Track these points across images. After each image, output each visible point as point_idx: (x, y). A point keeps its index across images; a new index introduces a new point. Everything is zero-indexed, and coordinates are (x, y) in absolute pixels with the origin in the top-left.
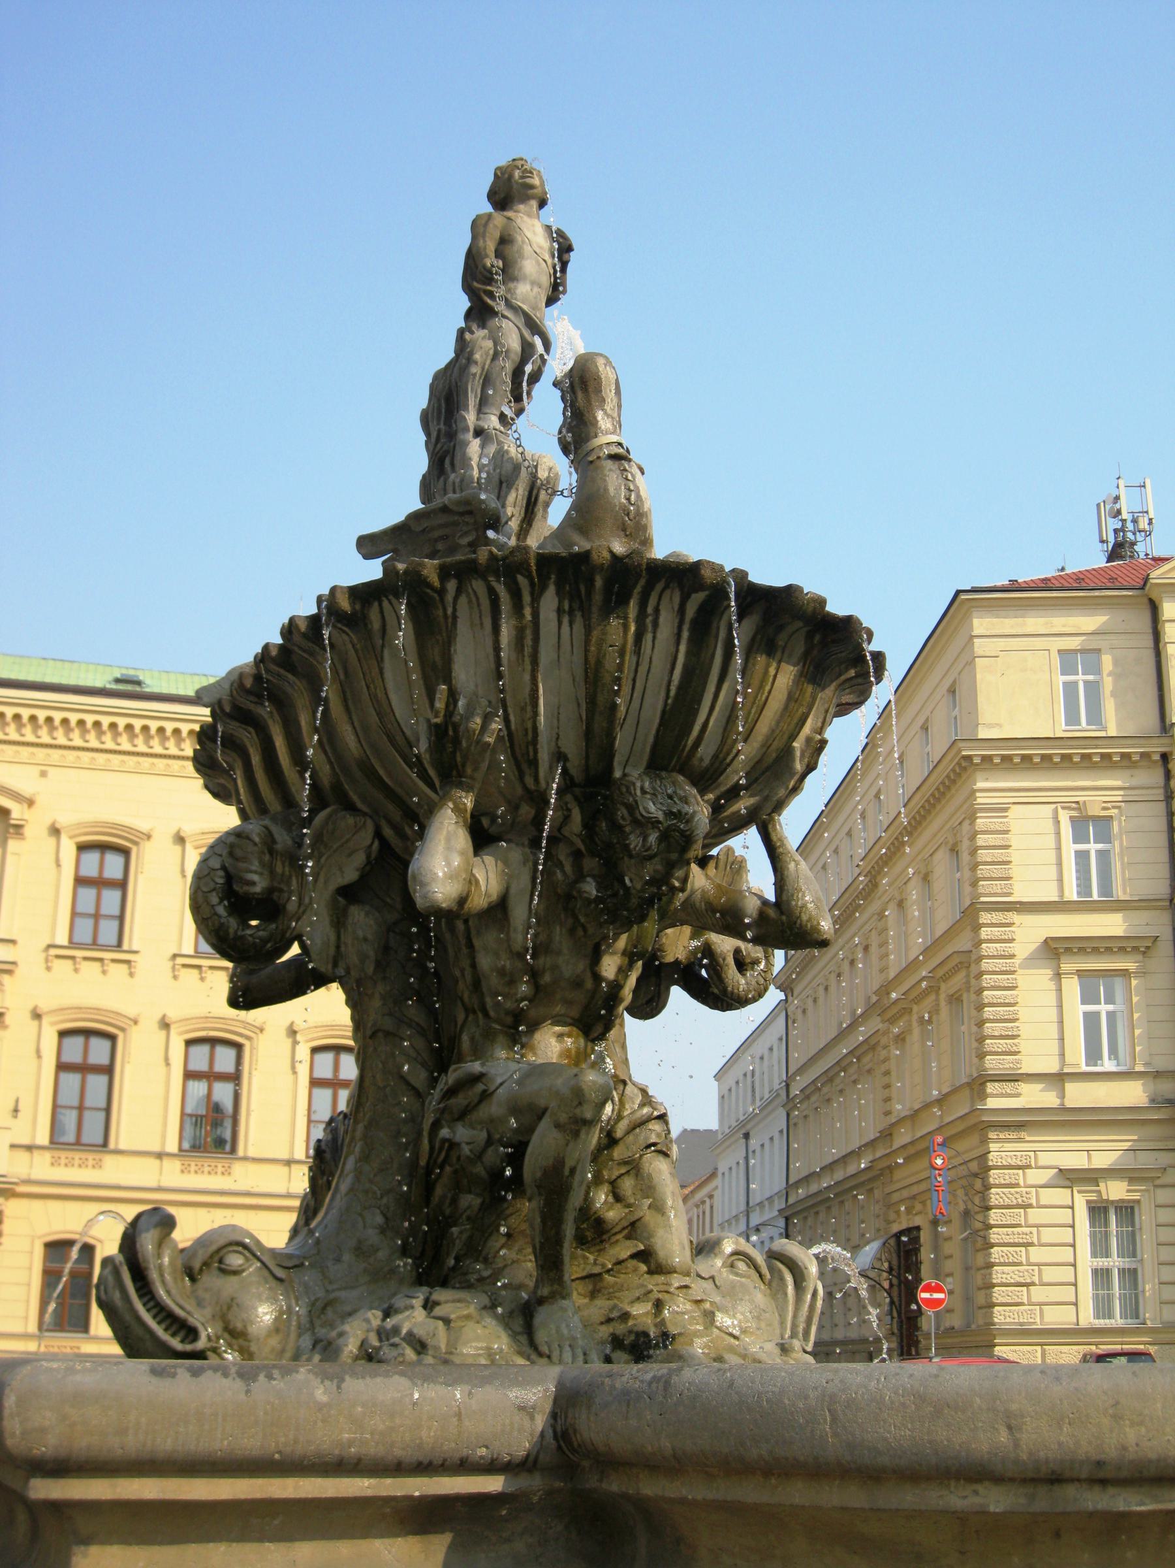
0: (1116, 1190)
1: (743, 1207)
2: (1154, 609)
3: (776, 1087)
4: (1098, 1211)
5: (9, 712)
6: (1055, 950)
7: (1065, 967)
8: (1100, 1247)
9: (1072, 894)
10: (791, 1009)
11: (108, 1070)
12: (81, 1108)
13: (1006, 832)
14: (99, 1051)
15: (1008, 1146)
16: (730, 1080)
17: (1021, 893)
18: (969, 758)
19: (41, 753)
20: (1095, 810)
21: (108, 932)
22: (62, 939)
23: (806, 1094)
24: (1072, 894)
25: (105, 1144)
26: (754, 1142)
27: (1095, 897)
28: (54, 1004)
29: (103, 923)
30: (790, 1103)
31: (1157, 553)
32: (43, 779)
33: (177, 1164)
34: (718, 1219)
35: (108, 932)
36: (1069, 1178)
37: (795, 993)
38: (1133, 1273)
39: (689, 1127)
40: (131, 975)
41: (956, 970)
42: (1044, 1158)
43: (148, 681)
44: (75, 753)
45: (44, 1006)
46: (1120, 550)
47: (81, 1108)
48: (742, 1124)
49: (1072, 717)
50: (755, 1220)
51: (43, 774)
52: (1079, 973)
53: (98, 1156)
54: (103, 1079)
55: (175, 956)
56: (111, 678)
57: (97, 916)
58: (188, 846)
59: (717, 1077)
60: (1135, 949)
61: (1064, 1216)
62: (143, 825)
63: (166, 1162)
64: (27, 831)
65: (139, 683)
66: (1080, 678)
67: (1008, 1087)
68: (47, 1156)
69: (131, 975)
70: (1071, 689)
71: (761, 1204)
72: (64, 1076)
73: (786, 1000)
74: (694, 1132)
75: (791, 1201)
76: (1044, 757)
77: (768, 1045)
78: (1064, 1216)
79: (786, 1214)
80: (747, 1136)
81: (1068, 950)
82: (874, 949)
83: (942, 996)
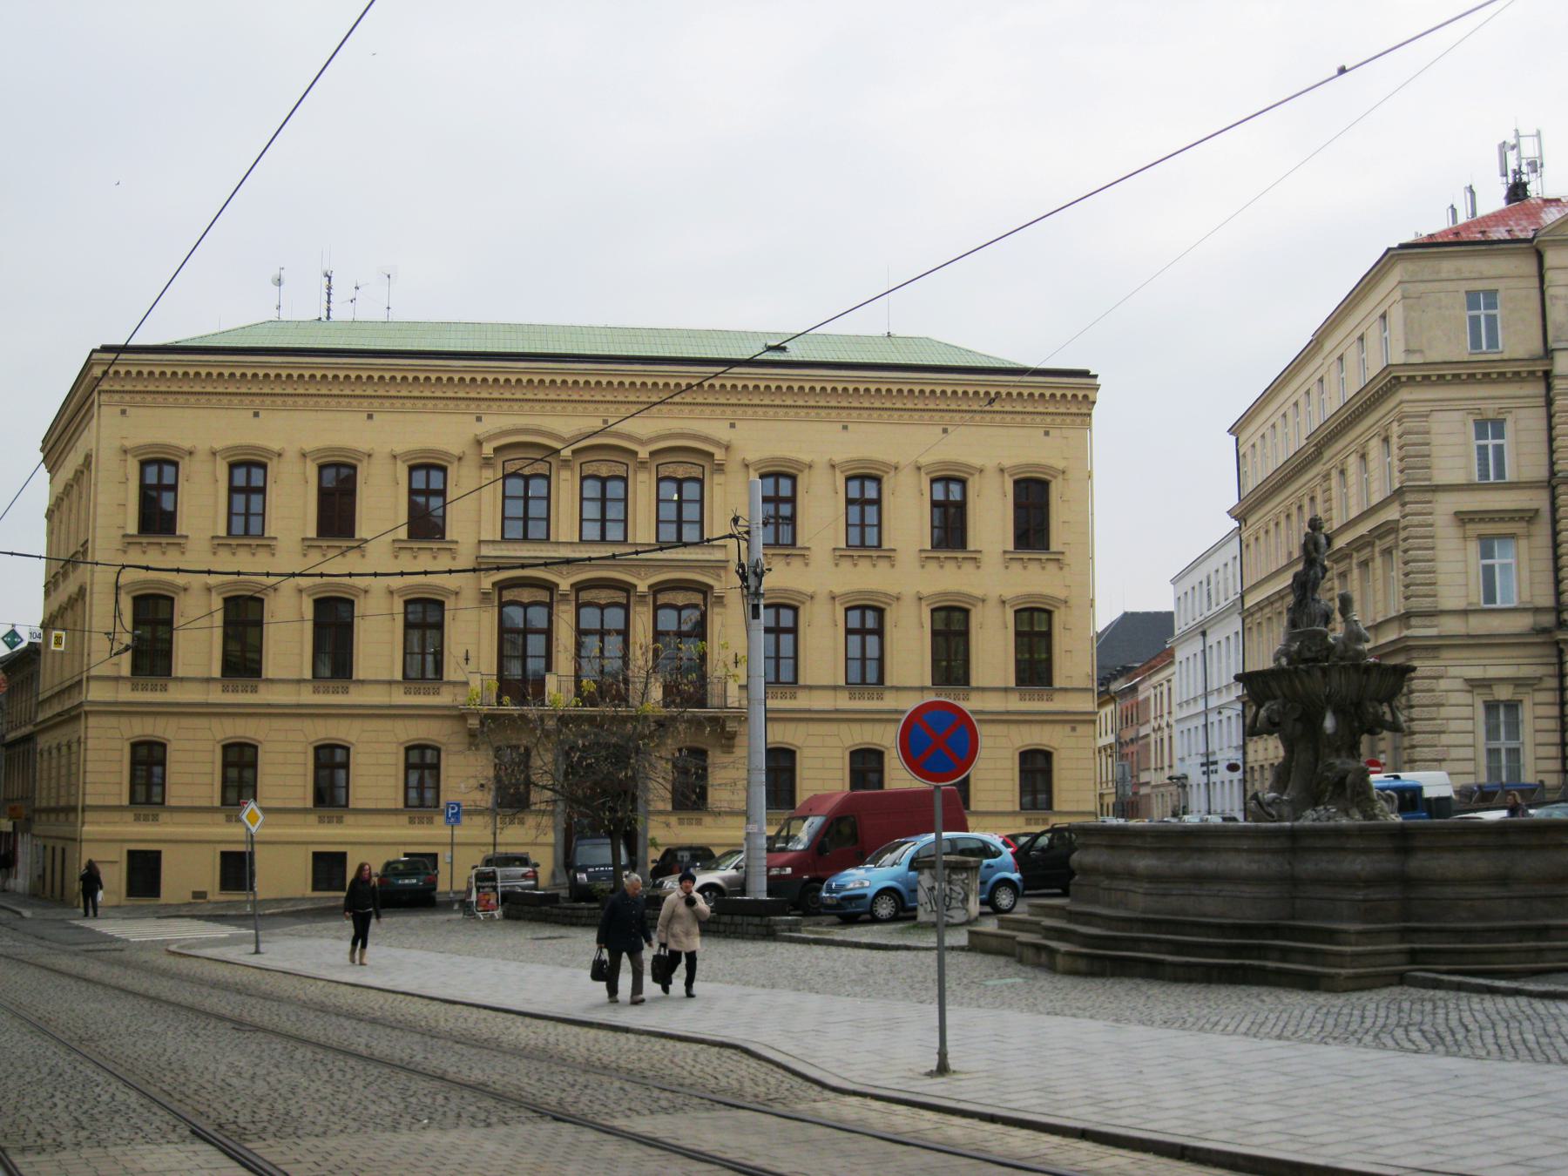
0: (1503, 693)
1: (1200, 691)
2: (1540, 257)
4: (1491, 707)
6: (1464, 518)
7: (1469, 533)
8: (1492, 733)
9: (1476, 479)
13: (1428, 433)
15: (1428, 663)
16: (1187, 584)
17: (1440, 478)
18: (1397, 378)
20: (1491, 415)
23: (1260, 606)
24: (1476, 479)
25: (796, 681)
26: (1212, 639)
27: (1492, 479)
30: (1246, 614)
31: (1549, 195)
34: (1175, 699)
36: (1474, 685)
38: (1517, 751)
39: (1131, 609)
41: (1388, 533)
42: (1453, 671)
46: (1517, 192)
48: (1201, 624)
49: (1476, 343)
50: (1214, 702)
52: (1480, 537)
54: (790, 637)
59: (1174, 581)
60: (1522, 519)
61: (1467, 712)
62: (805, 457)
63: (394, 687)
64: (728, 468)
66: (1482, 313)
67: (1427, 621)
70: (1475, 321)
71: (1219, 690)
72: (261, 484)
74: (1133, 614)
76: (1454, 376)
78: (1467, 712)
80: (1204, 634)
81: (1472, 520)
82: (1319, 500)
83: (1377, 550)
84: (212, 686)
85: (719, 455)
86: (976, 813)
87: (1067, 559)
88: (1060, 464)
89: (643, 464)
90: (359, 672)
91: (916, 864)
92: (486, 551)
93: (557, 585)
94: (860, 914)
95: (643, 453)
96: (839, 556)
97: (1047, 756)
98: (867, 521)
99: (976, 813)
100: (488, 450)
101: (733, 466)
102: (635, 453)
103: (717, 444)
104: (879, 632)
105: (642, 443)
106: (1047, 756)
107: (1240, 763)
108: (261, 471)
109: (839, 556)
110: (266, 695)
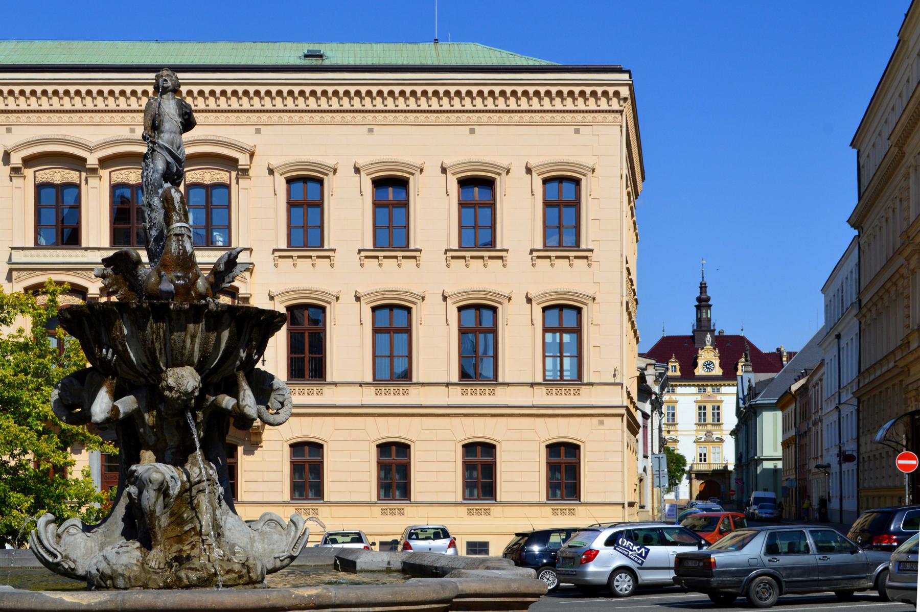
3: (854, 300)
5: (5, 89)
10: (862, 242)
11: (408, 331)
12: (391, 356)
14: (399, 318)
19: (254, 117)
21: (568, 239)
22: (540, 246)
28: (282, 289)
29: (480, 231)
32: (258, 135)
33: (372, 389)
35: (568, 239)
37: (865, 230)
40: (332, 266)
43: (328, 53)
44: (268, 114)
45: (275, 292)
47: (391, 356)
51: (258, 131)
53: (319, 387)
55: (360, 251)
56: (301, 54)
57: (305, 227)
58: (534, 174)
62: (415, 160)
63: (536, 389)
65: (321, 56)
68: (459, 389)
69: (504, 266)
72: (378, 336)
73: (859, 236)
75: (861, 385)
77: (850, 270)
79: (858, 395)
84: (537, 389)
85: (243, 160)
86: (243, 503)
87: (594, 256)
88: (589, 162)
89: (93, 171)
90: (332, 373)
91: (854, 551)
92: (18, 257)
93: (87, 289)
94: (735, 595)
95: (92, 160)
96: (451, 256)
97: (317, 447)
98: (565, 223)
99: (243, 503)
100: (16, 160)
101: (258, 170)
102: (84, 160)
103: (241, 149)
104: (577, 331)
105: (91, 150)
106: (317, 447)
107: (855, 454)
108: (318, 186)
109: (451, 256)
110: (415, 396)
